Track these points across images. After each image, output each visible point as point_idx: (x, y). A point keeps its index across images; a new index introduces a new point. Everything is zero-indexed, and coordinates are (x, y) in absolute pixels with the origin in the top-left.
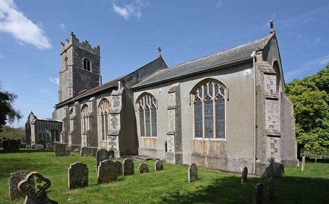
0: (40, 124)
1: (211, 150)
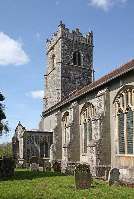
0: (29, 136)
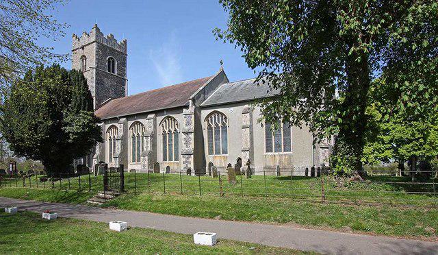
1: (280, 162)
